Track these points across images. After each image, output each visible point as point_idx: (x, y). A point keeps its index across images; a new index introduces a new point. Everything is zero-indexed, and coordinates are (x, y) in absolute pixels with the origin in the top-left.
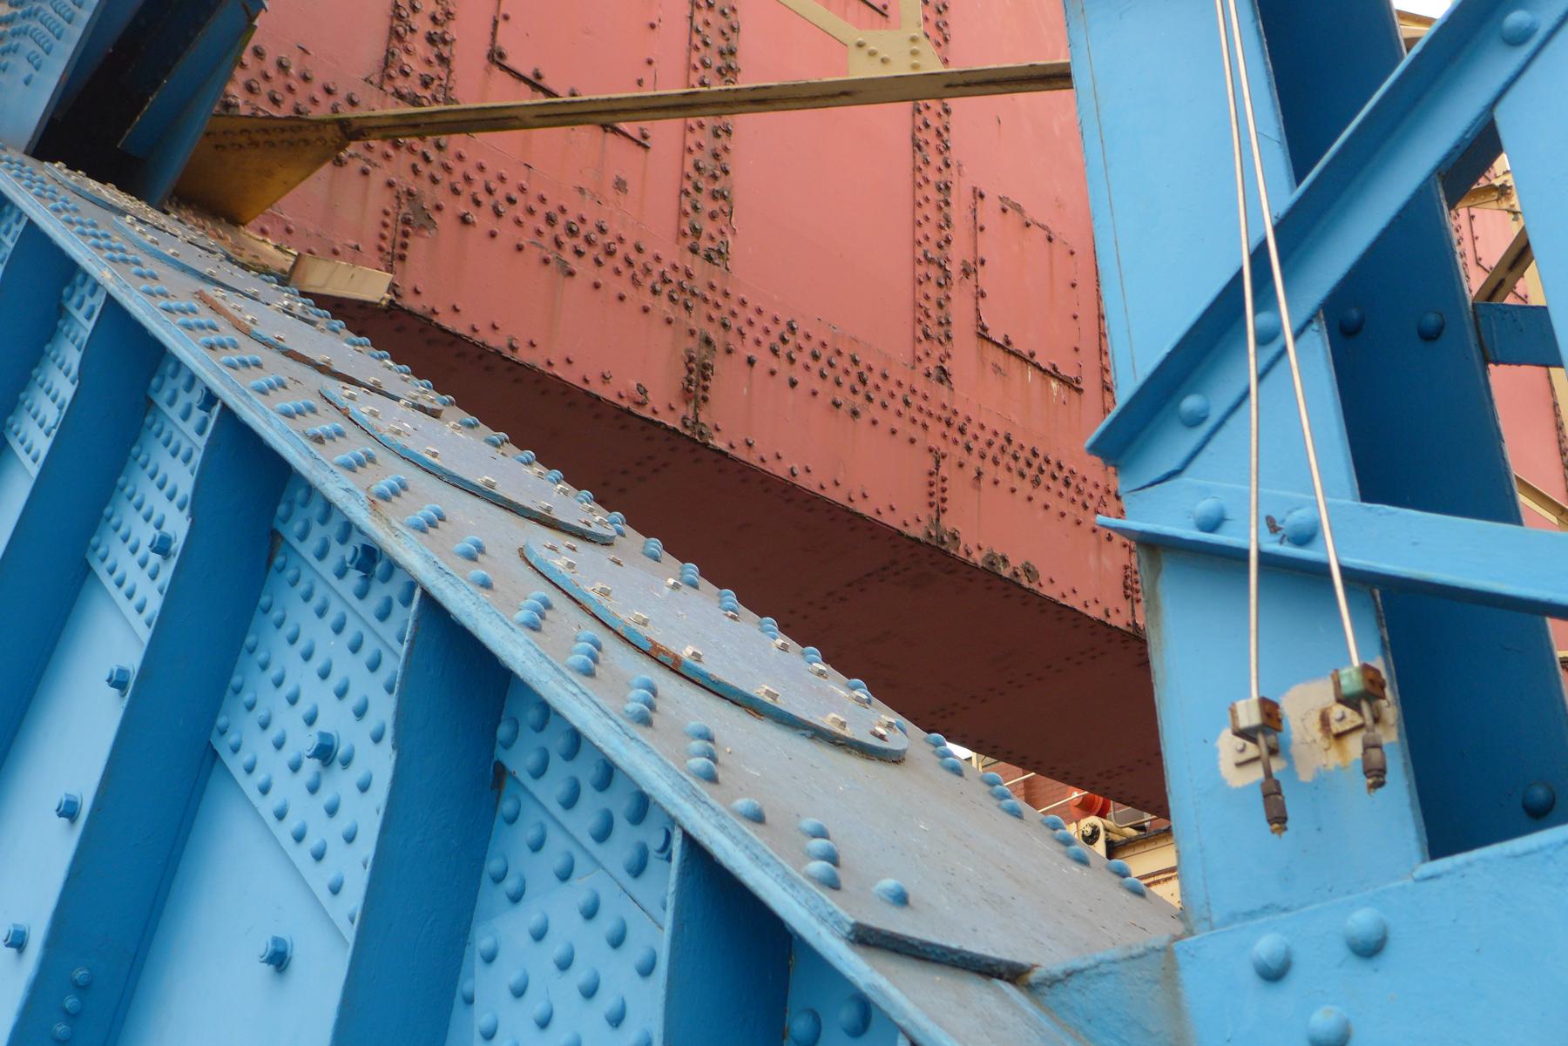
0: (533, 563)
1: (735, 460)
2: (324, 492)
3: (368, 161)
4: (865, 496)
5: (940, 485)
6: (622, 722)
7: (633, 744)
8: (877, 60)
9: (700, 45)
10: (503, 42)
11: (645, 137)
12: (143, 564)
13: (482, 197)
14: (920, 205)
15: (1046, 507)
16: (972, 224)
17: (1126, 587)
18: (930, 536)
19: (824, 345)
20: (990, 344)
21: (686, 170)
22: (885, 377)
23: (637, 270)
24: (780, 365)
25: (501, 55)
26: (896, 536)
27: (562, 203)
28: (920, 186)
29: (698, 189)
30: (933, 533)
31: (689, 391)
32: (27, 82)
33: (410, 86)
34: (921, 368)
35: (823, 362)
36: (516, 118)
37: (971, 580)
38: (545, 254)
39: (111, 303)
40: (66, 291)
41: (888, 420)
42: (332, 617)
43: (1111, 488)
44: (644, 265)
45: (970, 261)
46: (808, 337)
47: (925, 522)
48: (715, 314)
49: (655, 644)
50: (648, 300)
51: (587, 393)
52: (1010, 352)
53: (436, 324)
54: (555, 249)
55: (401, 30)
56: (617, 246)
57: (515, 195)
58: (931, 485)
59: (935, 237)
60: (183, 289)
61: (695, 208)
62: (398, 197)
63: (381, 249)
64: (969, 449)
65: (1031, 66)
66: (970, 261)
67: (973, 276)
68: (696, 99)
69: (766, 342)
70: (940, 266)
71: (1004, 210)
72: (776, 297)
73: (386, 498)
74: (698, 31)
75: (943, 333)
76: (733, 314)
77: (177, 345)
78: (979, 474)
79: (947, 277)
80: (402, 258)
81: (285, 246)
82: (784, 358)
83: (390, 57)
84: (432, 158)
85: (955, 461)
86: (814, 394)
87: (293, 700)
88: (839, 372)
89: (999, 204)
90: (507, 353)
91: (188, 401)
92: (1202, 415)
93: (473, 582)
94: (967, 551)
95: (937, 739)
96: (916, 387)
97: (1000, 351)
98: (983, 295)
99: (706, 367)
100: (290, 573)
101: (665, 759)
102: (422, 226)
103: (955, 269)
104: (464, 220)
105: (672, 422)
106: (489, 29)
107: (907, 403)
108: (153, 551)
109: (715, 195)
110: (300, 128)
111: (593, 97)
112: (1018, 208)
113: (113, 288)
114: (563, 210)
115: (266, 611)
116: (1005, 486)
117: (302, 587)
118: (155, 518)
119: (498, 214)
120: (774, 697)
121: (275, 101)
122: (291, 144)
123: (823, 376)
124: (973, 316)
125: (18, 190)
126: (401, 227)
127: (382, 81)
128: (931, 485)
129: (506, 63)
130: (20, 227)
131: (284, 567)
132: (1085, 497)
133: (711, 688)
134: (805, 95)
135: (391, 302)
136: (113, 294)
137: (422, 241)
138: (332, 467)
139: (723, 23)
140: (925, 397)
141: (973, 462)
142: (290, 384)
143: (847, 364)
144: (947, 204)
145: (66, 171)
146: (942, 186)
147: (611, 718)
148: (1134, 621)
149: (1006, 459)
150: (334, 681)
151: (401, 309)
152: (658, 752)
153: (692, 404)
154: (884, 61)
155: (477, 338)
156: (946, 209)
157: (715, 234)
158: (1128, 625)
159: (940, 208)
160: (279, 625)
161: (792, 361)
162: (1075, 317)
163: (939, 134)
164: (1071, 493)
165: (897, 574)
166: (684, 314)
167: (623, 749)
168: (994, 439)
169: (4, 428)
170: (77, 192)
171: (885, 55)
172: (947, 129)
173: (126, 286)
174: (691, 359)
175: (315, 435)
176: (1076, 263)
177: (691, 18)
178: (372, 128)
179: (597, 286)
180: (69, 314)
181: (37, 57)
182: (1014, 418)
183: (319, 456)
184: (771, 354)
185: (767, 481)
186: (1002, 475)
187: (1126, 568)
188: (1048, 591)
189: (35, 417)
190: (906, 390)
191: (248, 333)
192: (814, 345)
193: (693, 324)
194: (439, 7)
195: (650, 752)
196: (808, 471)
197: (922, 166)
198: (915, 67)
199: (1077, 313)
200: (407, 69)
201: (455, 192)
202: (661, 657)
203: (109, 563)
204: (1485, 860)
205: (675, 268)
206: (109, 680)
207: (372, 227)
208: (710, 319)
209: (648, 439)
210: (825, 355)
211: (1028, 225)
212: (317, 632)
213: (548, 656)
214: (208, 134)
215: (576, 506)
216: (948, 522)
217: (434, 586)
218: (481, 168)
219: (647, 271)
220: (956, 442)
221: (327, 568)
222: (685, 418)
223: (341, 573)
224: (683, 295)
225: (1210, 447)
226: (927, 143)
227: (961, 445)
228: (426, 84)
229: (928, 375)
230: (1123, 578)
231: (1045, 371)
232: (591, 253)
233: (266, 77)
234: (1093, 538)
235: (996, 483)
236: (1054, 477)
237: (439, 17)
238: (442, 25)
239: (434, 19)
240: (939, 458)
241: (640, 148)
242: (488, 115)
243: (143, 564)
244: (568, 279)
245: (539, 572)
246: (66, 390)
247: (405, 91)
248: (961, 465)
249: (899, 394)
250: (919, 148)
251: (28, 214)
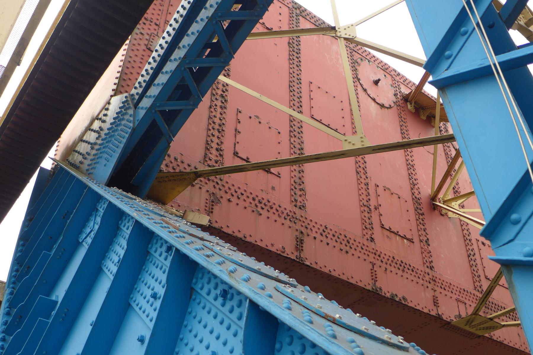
0: (280, 291)
1: (312, 268)
2: (212, 272)
3: (201, 185)
4: (352, 278)
5: (375, 273)
6: (328, 337)
7: (333, 345)
8: (351, 144)
9: (293, 147)
10: (237, 149)
11: (279, 174)
12: (148, 302)
13: (234, 193)
14: (360, 189)
15: (407, 278)
16: (376, 194)
17: (434, 302)
18: (373, 289)
19: (336, 232)
20: (385, 230)
21: (292, 183)
22: (355, 241)
23: (280, 212)
24: (324, 239)
25: (237, 153)
26: (363, 290)
27: (257, 194)
28: (360, 184)
29: (295, 188)
30: (374, 288)
31: (297, 248)
32: (105, 166)
33: (212, 163)
34: (365, 238)
35: (336, 237)
36: (246, 168)
37: (386, 302)
38: (253, 209)
39: (138, 224)
40: (120, 222)
41: (357, 254)
42: (213, 313)
43: (426, 272)
44: (282, 211)
45: (376, 205)
46: (331, 230)
47: (371, 285)
48: (303, 224)
49: (326, 314)
50: (283, 221)
51: (267, 250)
52: (391, 232)
53: (223, 231)
54: (255, 207)
55: (209, 147)
56: (273, 206)
57: (243, 193)
58: (372, 273)
59: (365, 199)
60: (158, 219)
61: (295, 194)
62: (210, 195)
63: (206, 210)
64: (382, 261)
65: (398, 142)
66: (376, 205)
67: (378, 210)
68: (299, 159)
69: (319, 232)
70: (368, 207)
71: (385, 190)
72: (321, 219)
73: (233, 272)
74: (292, 144)
75: (370, 227)
76: (309, 224)
77: (160, 233)
78: (386, 269)
79: (370, 210)
80: (212, 212)
81: (178, 210)
82: (324, 236)
83: (206, 155)
84: (219, 183)
85: (378, 265)
86: (334, 247)
87: (201, 341)
88: (341, 240)
89: (383, 188)
90: (244, 239)
91: (161, 250)
92: (519, 220)
93: (267, 296)
94: (385, 293)
95: (413, 345)
96: (364, 243)
97: (388, 232)
98: (381, 215)
99: (302, 240)
100: (198, 301)
101: (346, 349)
102: (217, 203)
103: (372, 208)
104: (229, 200)
105: (293, 257)
106: (233, 146)
107: (362, 248)
108: (151, 297)
109: (301, 190)
110: (183, 175)
111: (268, 161)
112: (389, 189)
113: (137, 218)
114: (257, 196)
115: (190, 313)
116: (394, 272)
117: (202, 305)
118: (151, 287)
119: (239, 198)
120: (367, 330)
121: (174, 169)
122: (180, 180)
123: (336, 241)
124: (379, 221)
125: (105, 193)
126: (211, 203)
127: (204, 162)
128: (372, 273)
129: (239, 155)
130: (106, 205)
131: (195, 299)
132: (419, 275)
133: (346, 327)
134: (331, 155)
135: (209, 225)
136: (137, 219)
137: (217, 207)
138: (214, 264)
139: (299, 141)
140: (367, 246)
141: (384, 266)
142: (194, 243)
143: (344, 238)
144: (368, 189)
145: (117, 189)
146: (366, 184)
147: (324, 337)
148: (438, 313)
149: (394, 264)
150: (215, 334)
151: (212, 227)
152: (343, 347)
153: (299, 252)
154: (353, 144)
155: (235, 235)
156: (368, 190)
157: (301, 201)
158: (436, 314)
159: (366, 190)
160: (195, 317)
162: (409, 220)
163: (364, 169)
164: (414, 274)
165: (363, 301)
166: (294, 225)
167: (330, 347)
168: (389, 258)
169: (101, 264)
170: (121, 194)
171: (354, 143)
172: (366, 167)
173: (141, 217)
174: (297, 238)
175: (207, 255)
176: (408, 204)
177: (290, 140)
178: (204, 174)
179: (268, 218)
180: (121, 229)
181: (108, 158)
182: (395, 252)
183: (209, 261)
184: (320, 236)
185: (322, 274)
186: (392, 269)
187: (434, 296)
188: (410, 305)
189: (111, 260)
190: (361, 245)
191: (178, 229)
192: (333, 232)
193: (297, 228)
194: (219, 141)
195: (340, 347)
196: (335, 270)
197: (360, 178)
198: (363, 145)
199: (410, 219)
200: (211, 158)
201: (226, 192)
202: (329, 318)
203: (136, 302)
205: (290, 211)
206: (138, 339)
207: (203, 204)
208: (302, 226)
209: (286, 263)
210: (336, 235)
211: (392, 194)
212: (208, 319)
213: (297, 318)
214: (156, 178)
215: (283, 277)
216: (378, 285)
217: (254, 298)
218: (233, 185)
219: (283, 213)
220: (378, 260)
221: (211, 298)
222: (297, 256)
223: (216, 299)
224: (294, 219)
225: (524, 230)
226: (360, 172)
227: (380, 260)
228: (216, 162)
229: (368, 240)
230: (433, 300)
231: (402, 237)
232: (266, 208)
233: (171, 162)
234: (422, 287)
235: (391, 271)
236: (409, 269)
237: (219, 143)
238: (220, 146)
239: (218, 144)
240: (374, 265)
241: (278, 178)
242: (238, 168)
243: (148, 302)
244: (260, 216)
245: (282, 294)
246: (122, 253)
247: (211, 165)
248: (380, 267)
249: (360, 245)
250: (358, 173)
251: (109, 200)
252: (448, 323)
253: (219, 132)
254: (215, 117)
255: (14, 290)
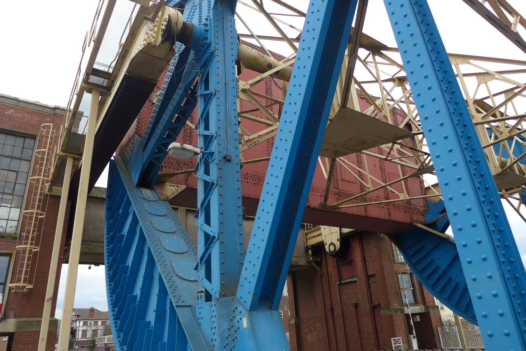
35: (253, 178)
161: (247, 179)
204: (80, 193)
252: (314, 209)
253: (190, 137)
254: (187, 129)
255: (109, 223)
